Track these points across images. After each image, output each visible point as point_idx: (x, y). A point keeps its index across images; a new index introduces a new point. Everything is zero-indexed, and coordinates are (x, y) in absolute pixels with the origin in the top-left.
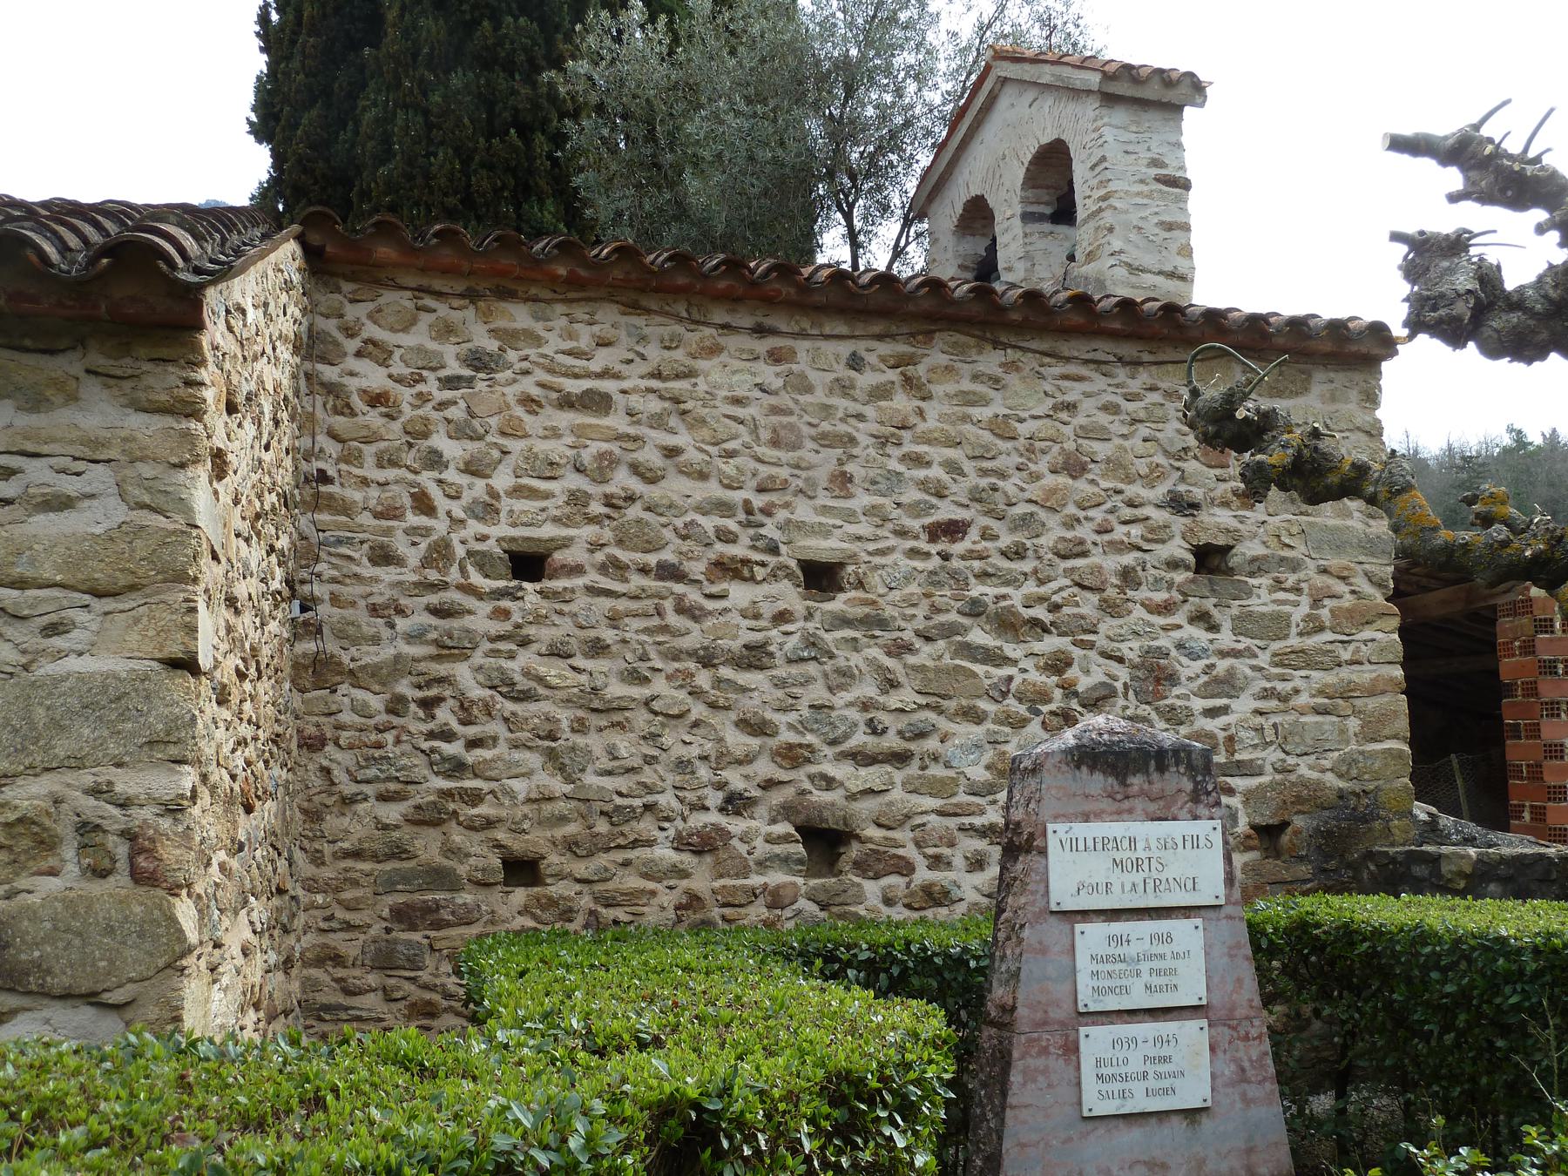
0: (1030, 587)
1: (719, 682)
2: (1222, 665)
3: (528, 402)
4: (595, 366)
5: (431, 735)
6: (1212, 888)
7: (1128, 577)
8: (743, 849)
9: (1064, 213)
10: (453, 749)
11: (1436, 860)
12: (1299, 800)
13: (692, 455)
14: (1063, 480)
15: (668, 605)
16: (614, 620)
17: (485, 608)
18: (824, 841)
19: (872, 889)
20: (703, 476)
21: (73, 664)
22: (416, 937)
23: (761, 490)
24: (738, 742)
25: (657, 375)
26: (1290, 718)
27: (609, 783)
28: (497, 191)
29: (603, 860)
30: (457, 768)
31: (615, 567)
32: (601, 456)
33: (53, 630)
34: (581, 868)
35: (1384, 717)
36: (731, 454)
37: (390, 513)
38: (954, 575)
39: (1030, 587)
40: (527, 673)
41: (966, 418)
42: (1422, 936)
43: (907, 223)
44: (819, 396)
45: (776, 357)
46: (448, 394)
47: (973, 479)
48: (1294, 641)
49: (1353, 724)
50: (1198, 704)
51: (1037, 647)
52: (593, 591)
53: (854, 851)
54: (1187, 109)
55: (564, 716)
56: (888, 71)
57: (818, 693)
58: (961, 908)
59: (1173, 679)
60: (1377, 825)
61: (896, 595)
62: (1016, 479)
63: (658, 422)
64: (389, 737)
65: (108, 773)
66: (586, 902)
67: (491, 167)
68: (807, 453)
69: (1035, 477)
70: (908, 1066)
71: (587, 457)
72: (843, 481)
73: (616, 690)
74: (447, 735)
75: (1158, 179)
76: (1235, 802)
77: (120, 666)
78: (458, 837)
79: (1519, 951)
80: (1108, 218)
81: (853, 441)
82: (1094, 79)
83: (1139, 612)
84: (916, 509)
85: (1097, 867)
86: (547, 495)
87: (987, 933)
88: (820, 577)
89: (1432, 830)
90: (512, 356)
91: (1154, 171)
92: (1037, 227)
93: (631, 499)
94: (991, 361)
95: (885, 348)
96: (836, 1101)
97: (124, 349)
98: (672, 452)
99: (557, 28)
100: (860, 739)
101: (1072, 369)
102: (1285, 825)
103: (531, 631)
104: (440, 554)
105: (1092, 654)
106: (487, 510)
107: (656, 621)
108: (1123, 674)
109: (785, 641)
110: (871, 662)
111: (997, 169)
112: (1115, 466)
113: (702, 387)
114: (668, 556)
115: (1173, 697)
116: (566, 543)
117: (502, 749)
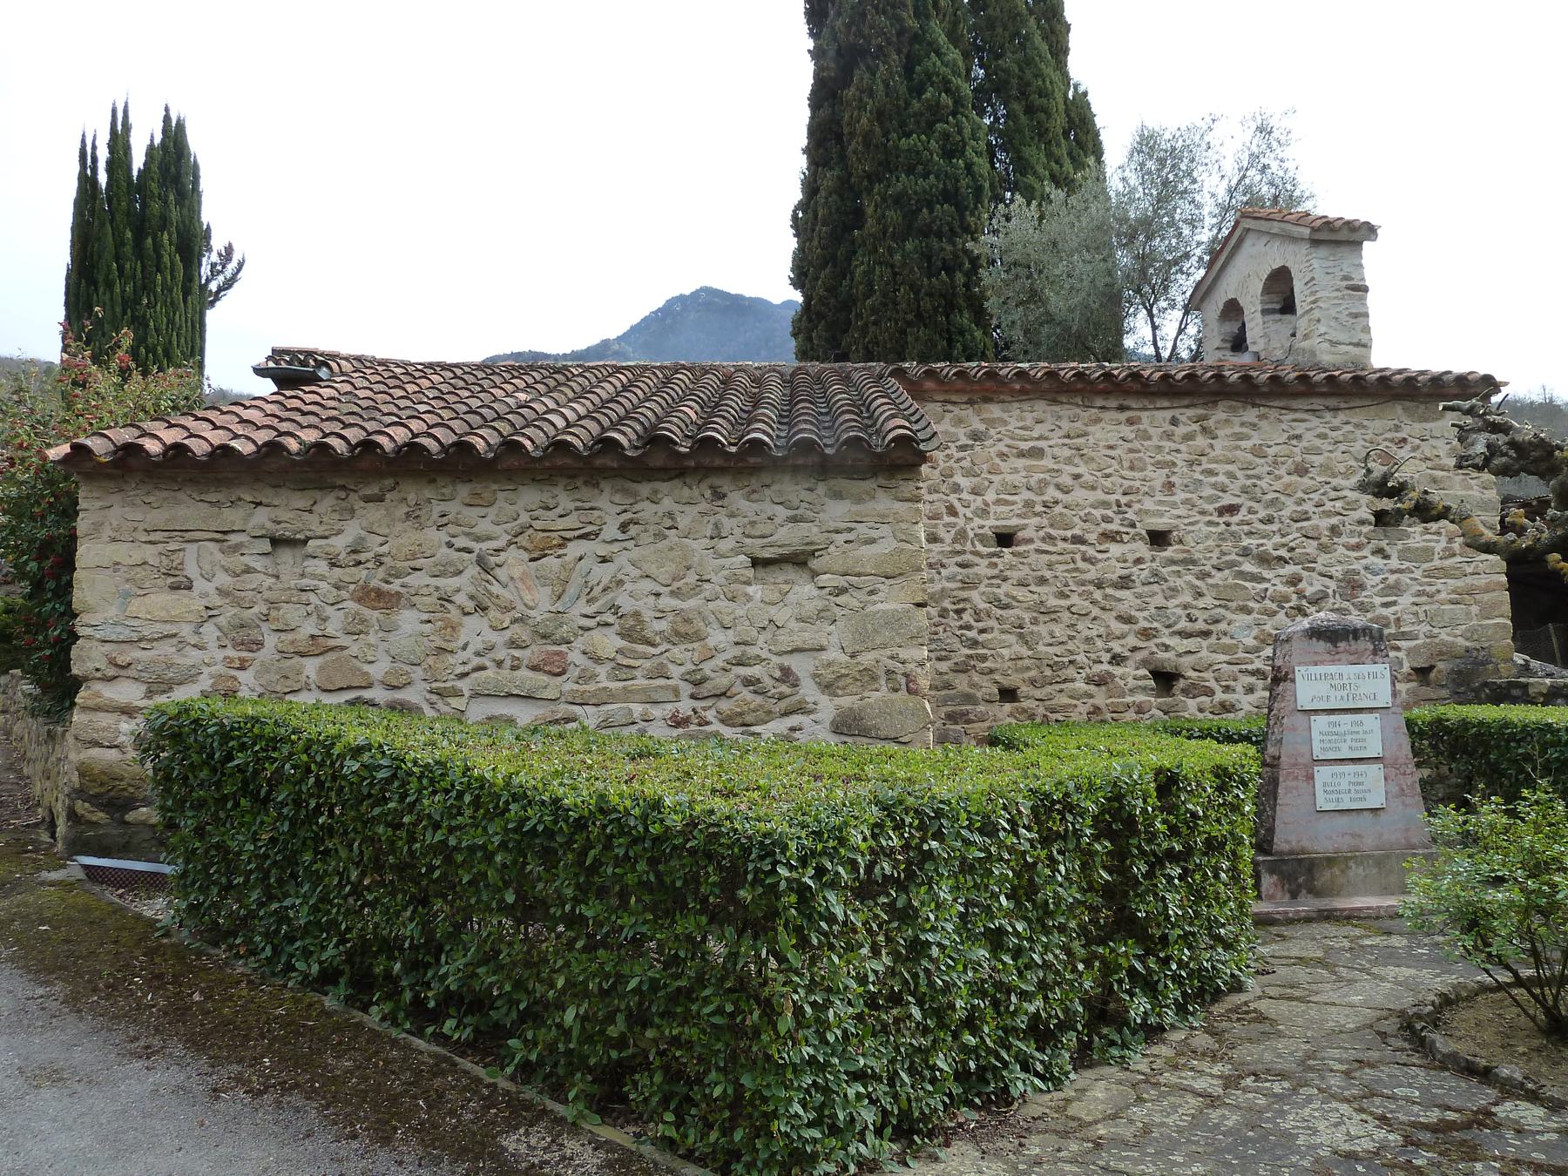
0: (1277, 539)
1: (1106, 597)
2: (1392, 578)
3: (1002, 455)
4: (1035, 434)
5: (961, 628)
6: (1385, 699)
7: (1334, 530)
8: (1122, 683)
9: (1288, 307)
10: (972, 634)
11: (1526, 686)
12: (1441, 653)
13: (1087, 478)
14: (1295, 478)
15: (1078, 557)
16: (1050, 566)
17: (985, 562)
18: (1165, 679)
19: (1192, 704)
20: (1093, 488)
21: (880, 606)
22: (958, 727)
23: (1125, 494)
24: (1118, 627)
25: (1068, 437)
26: (1435, 607)
27: (1051, 650)
28: (935, 309)
29: (1049, 689)
30: (975, 643)
31: (1050, 538)
32: (1040, 481)
33: (872, 593)
34: (1038, 693)
35: (1495, 605)
36: (1108, 476)
37: (935, 516)
38: (1232, 534)
39: (1277, 539)
40: (1007, 595)
41: (1237, 448)
42: (1507, 724)
43: (1186, 313)
44: (1155, 441)
45: (1130, 422)
46: (962, 454)
47: (1243, 481)
48: (1437, 563)
49: (1475, 609)
50: (1378, 600)
51: (1282, 572)
52: (1038, 551)
53: (1181, 683)
54: (1366, 244)
55: (1027, 616)
56: (1172, 223)
57: (1159, 600)
58: (1241, 714)
59: (1362, 587)
60: (1490, 667)
61: (1200, 547)
62: (1268, 479)
63: (1069, 461)
64: (941, 629)
65: (896, 650)
66: (1041, 710)
67: (930, 295)
68: (1148, 473)
69: (1279, 478)
70: (1243, 766)
71: (1033, 482)
72: (1169, 486)
73: (1053, 602)
74: (969, 628)
75: (1347, 288)
76: (1401, 655)
77: (899, 607)
78: (976, 678)
79: (1559, 730)
80: (1316, 314)
81: (1174, 464)
82: (1307, 231)
83: (1341, 550)
84: (1211, 499)
85: (1322, 688)
86: (1013, 503)
87: (1263, 724)
88: (1158, 539)
89: (1526, 669)
90: (992, 432)
91: (1345, 283)
92: (1271, 317)
93: (1056, 502)
94: (1251, 415)
95: (1190, 412)
96: (1217, 776)
97: (892, 477)
98: (1077, 477)
99: (966, 208)
100: (1183, 624)
101: (1298, 415)
102: (1432, 667)
103: (1008, 573)
104: (961, 536)
105: (1314, 574)
106: (984, 512)
107: (1072, 566)
108: (1332, 585)
109: (1140, 574)
110: (1188, 583)
111: (1245, 281)
112: (1326, 468)
113: (1092, 440)
114: (1077, 531)
115: (1363, 597)
116: (1024, 527)
117: (996, 634)
